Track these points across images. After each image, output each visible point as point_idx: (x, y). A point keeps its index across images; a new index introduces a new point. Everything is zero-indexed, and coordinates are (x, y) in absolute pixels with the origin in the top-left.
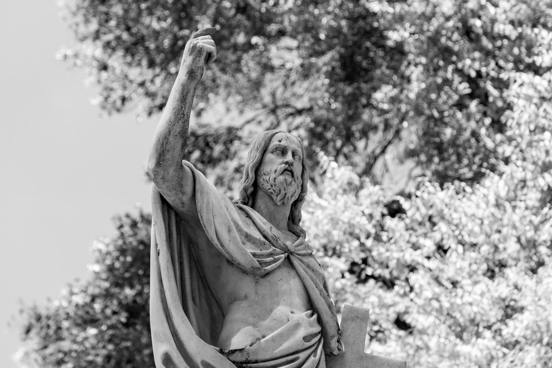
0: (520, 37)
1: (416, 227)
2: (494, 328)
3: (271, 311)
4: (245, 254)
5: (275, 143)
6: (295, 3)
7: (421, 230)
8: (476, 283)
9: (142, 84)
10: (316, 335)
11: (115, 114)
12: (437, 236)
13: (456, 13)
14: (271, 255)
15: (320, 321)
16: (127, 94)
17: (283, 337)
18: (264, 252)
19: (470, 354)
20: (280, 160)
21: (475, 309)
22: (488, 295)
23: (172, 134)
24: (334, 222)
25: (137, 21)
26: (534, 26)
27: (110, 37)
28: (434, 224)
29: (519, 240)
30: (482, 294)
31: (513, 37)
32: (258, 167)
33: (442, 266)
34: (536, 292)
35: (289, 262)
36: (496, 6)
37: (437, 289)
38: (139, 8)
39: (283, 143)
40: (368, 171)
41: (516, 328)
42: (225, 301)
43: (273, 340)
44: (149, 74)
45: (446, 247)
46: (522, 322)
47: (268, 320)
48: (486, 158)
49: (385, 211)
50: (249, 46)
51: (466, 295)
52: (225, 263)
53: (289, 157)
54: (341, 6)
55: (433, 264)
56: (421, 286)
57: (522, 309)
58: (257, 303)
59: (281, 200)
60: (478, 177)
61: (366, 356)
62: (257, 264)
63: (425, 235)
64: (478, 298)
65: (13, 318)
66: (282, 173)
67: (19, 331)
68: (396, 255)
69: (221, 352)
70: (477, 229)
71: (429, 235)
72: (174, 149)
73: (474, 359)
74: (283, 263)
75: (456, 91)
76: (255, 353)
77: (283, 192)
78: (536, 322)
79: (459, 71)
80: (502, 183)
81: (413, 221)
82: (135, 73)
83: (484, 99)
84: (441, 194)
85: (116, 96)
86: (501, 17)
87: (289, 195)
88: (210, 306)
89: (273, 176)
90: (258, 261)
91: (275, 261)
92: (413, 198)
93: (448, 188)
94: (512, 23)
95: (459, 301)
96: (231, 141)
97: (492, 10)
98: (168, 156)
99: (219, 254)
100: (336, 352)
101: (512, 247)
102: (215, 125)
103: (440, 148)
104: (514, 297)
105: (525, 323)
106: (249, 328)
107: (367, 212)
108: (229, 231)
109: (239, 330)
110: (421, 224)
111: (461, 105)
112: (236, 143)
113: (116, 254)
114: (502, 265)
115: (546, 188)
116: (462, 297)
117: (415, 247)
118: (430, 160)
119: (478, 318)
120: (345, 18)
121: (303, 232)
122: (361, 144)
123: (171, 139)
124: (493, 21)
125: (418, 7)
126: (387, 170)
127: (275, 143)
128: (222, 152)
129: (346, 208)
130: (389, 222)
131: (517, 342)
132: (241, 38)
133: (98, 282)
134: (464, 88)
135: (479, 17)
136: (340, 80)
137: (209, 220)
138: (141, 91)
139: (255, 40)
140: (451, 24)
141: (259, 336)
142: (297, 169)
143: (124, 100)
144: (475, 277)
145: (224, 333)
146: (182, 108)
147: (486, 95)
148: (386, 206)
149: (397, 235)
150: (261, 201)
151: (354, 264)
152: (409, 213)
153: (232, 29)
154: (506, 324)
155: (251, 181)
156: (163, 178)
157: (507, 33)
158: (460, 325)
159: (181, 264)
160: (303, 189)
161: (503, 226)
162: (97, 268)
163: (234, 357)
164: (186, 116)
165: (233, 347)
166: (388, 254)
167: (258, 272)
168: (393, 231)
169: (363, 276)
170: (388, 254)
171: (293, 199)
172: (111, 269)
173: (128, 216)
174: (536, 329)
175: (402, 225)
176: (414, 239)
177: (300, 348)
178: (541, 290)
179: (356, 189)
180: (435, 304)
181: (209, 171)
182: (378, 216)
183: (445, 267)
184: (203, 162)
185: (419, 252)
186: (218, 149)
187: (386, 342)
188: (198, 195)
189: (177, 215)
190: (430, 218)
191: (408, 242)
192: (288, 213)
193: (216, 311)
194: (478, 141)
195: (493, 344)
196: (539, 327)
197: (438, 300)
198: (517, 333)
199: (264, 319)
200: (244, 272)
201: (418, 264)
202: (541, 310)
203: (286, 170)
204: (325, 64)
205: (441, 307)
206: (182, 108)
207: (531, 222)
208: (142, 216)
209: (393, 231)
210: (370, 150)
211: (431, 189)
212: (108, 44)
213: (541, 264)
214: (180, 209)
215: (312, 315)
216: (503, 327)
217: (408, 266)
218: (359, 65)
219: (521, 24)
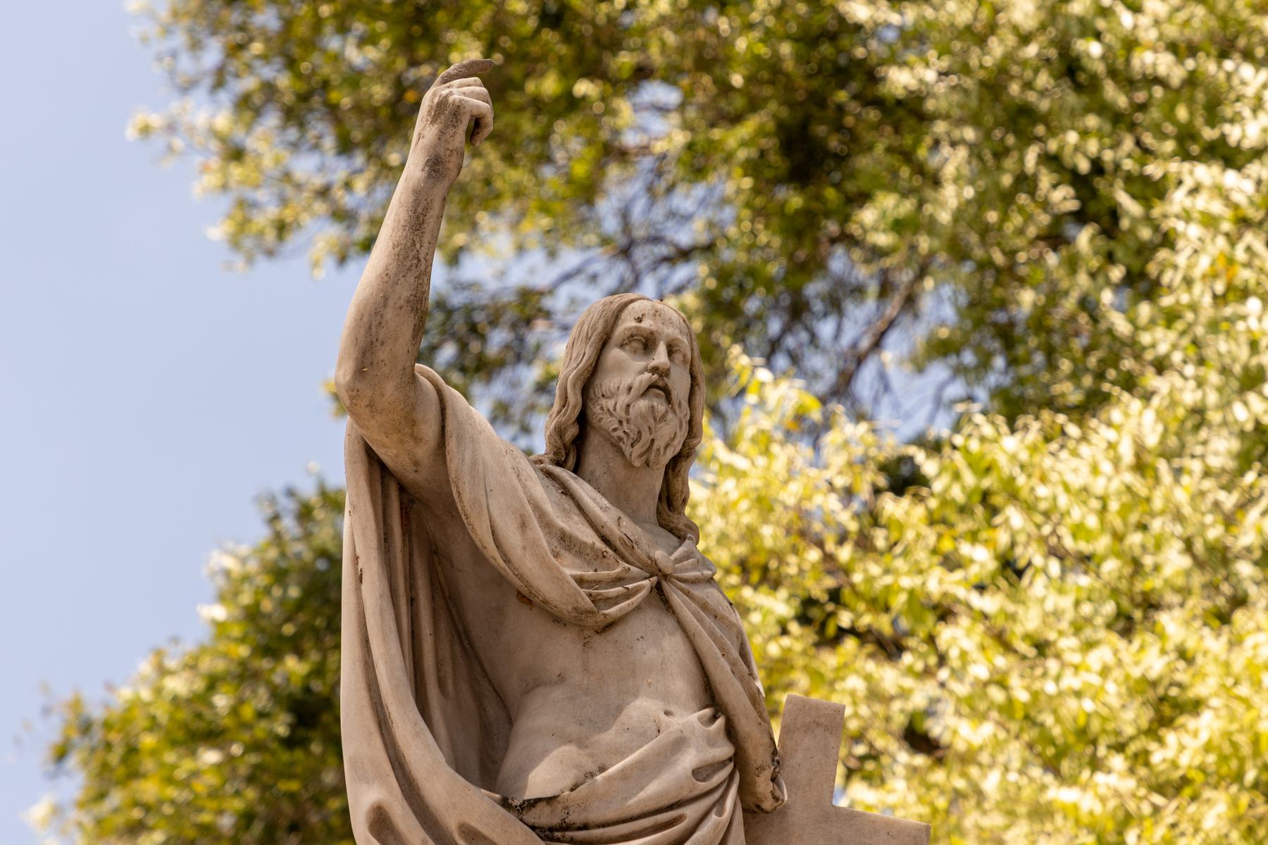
0: (1192, 80)
1: (953, 516)
2: (1133, 748)
3: (620, 709)
4: (559, 578)
5: (627, 323)
7: (963, 526)
8: (1090, 645)
9: (324, 193)
10: (723, 764)
11: (263, 264)
12: (1003, 538)
13: (1043, 27)
14: (618, 580)
15: (731, 732)
16: (288, 215)
17: (646, 770)
18: (603, 573)
19: (1076, 807)
20: (640, 364)
21: (1088, 705)
22: (1117, 674)
23: (391, 302)
25: (311, 44)
26: (1223, 55)
27: (249, 83)
28: (994, 511)
30: (1105, 672)
33: (1011, 608)
34: (1227, 665)
35: (659, 595)
36: (1136, 9)
37: (1001, 661)
39: (647, 324)
40: (842, 389)
41: (1182, 748)
43: (624, 775)
44: (339, 169)
46: (1195, 734)
47: (612, 731)
48: (1113, 360)
49: (882, 481)
50: (570, 104)
51: (1068, 673)
52: (514, 601)
53: (660, 357)
54: (778, 12)
55: (989, 603)
56: (964, 655)
57: (1196, 706)
59: (641, 455)
60: (1094, 403)
63: (974, 537)
64: (1095, 680)
66: (644, 394)
67: (40, 756)
68: (906, 582)
69: (505, 803)
70: (1092, 522)
71: (984, 535)
72: (397, 339)
73: (1085, 819)
74: (647, 601)
75: (1045, 205)
77: (646, 437)
78: (1227, 735)
79: (1052, 160)
80: (1149, 416)
81: (945, 502)
82: (305, 167)
84: (1011, 443)
86: (1151, 35)
87: (659, 444)
88: (478, 698)
89: (623, 399)
90: (590, 595)
91: (628, 595)
92: (947, 450)
93: (1026, 428)
94: (1173, 47)
95: (1050, 687)
96: (528, 322)
97: (1126, 18)
98: (383, 354)
99: (500, 580)
100: (768, 804)
101: (1175, 562)
102: (492, 285)
103: (1007, 336)
104: (1179, 677)
105: (1204, 737)
106: (569, 750)
107: (840, 482)
108: (523, 525)
110: (964, 510)
111: (1055, 238)
112: (540, 326)
114: (1151, 604)
115: (1249, 427)
116: (1057, 679)
117: (951, 563)
119: (1095, 726)
120: (788, 37)
122: (826, 329)
123: (389, 314)
124: (1131, 44)
126: (887, 387)
127: (627, 323)
128: (507, 347)
130: (892, 506)
131: (1185, 781)
132: (550, 85)
133: (222, 647)
135: (1098, 36)
136: (778, 181)
138: (320, 207)
139: (583, 88)
140: (1032, 50)
141: (591, 766)
142: (679, 383)
143: (282, 228)
144: (1088, 633)
146: (414, 244)
147: (1114, 213)
148: (883, 468)
149: (910, 535)
150: (596, 457)
152: (938, 486)
153: (533, 64)
155: (573, 412)
156: (371, 405)
157: (1162, 70)
158: (1052, 741)
159: (412, 601)
160: (693, 431)
162: (219, 612)
163: (535, 816)
164: (423, 261)
165: (530, 794)
166: (888, 580)
167: (590, 621)
168: (901, 527)
169: (831, 630)
170: (888, 580)
171: (670, 454)
172: (252, 615)
173: (291, 493)
174: (1227, 749)
175: (919, 512)
176: (947, 545)
177: (686, 794)
178: (1239, 662)
180: (997, 694)
181: (477, 389)
182: (864, 492)
183: (1020, 610)
184: (463, 369)
185: (958, 575)
188: (452, 444)
189: (402, 489)
191: (934, 551)
193: (492, 710)
195: (1129, 784)
196: (1235, 745)
198: (1184, 760)
199: (604, 728)
200: (557, 620)
201: (957, 601)
202: (1239, 708)
203: (652, 386)
204: (743, 144)
205: (1010, 701)
206: (414, 244)
207: (1217, 505)
209: (901, 527)
210: (846, 340)
211: (988, 430)
213: (1239, 601)
214: (409, 474)
215: (714, 718)
216: (1153, 746)
219: (1192, 50)
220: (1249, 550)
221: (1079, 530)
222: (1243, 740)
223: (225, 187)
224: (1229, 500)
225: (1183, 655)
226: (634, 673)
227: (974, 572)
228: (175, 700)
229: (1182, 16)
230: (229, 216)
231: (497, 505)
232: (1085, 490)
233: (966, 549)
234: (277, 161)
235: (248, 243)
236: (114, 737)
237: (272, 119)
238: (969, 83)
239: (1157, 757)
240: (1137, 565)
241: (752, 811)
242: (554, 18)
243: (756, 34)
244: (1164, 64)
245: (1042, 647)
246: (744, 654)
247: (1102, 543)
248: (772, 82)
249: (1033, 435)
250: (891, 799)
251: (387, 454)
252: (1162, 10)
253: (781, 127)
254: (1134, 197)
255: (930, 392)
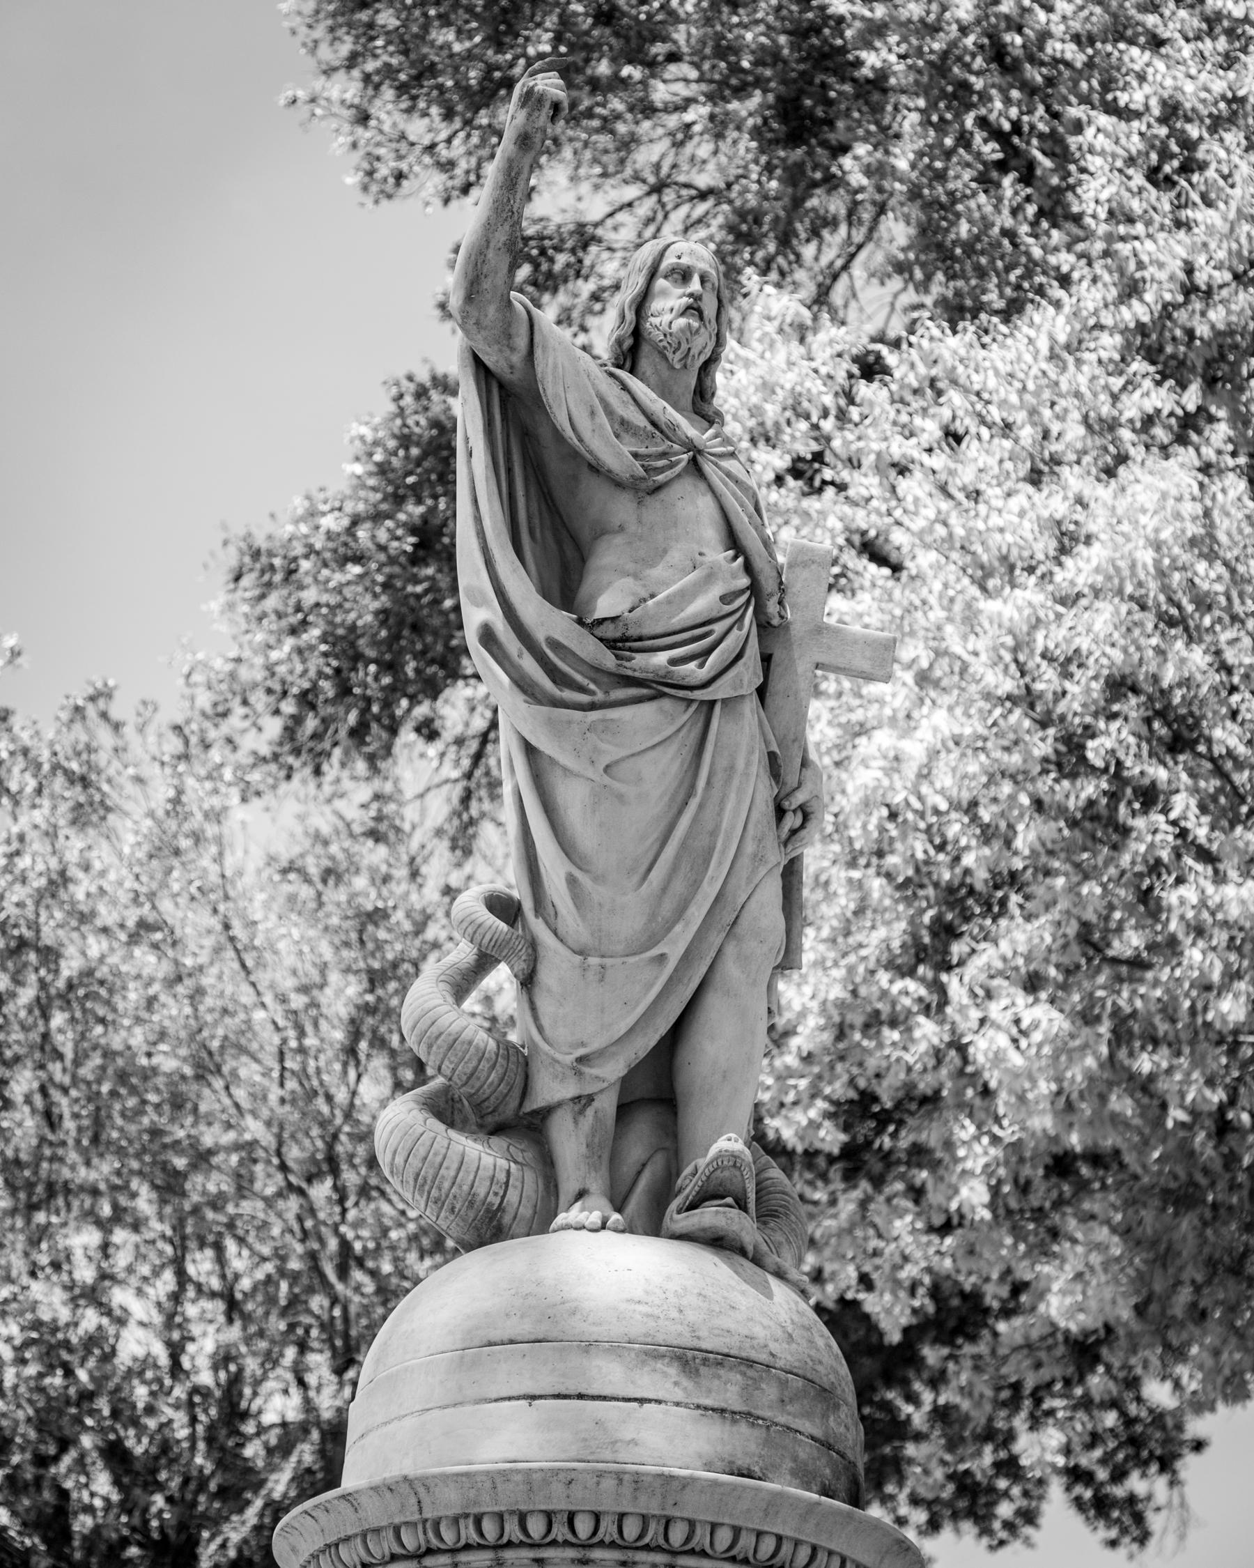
0: (1090, 64)
1: (909, 397)
3: (665, 551)
4: (619, 454)
5: (669, 261)
6: (697, 5)
7: (917, 404)
9: (431, 148)
11: (385, 203)
12: (946, 413)
13: (978, 22)
14: (664, 455)
15: (748, 568)
16: (404, 166)
17: (685, 596)
18: (652, 450)
19: (1000, 614)
20: (680, 291)
21: (1009, 538)
22: (1031, 515)
24: (768, 388)
25: (422, 37)
27: (371, 66)
28: (939, 393)
29: (1086, 420)
30: (1022, 514)
31: (1079, 65)
32: (641, 304)
33: (952, 465)
35: (695, 467)
36: (1049, 9)
37: (945, 505)
38: (425, 15)
39: (685, 261)
40: (821, 298)
42: (585, 534)
43: (669, 601)
45: (961, 431)
46: (1088, 560)
48: (1028, 275)
49: (855, 370)
50: (618, 83)
51: (994, 516)
52: (585, 469)
53: (695, 285)
54: (778, 9)
55: (938, 461)
56: (916, 500)
57: (1088, 540)
58: (641, 538)
60: (1012, 310)
61: (828, 628)
62: (641, 472)
64: (1016, 520)
65: (212, 554)
66: (683, 314)
67: (224, 576)
68: (875, 446)
69: (580, 622)
70: (1014, 399)
71: (932, 411)
73: (1007, 623)
74: (685, 469)
75: (978, 155)
76: (638, 623)
77: (684, 346)
78: (1112, 562)
79: (982, 122)
80: (1061, 320)
82: (417, 129)
83: (1028, 175)
84: (953, 341)
85: (383, 171)
86: (1059, 29)
87: (695, 351)
88: (559, 543)
89: (667, 318)
91: (672, 465)
92: (904, 346)
94: (1076, 38)
95: (981, 525)
96: (585, 247)
97: (1042, 16)
98: (486, 285)
99: (575, 455)
101: (1075, 432)
102: (557, 219)
104: (1076, 517)
105: (1094, 563)
106: (629, 582)
107: (823, 370)
109: (610, 584)
110: (915, 392)
111: (986, 182)
112: (593, 249)
113: (392, 444)
114: (1055, 461)
115: (1132, 325)
117: (909, 433)
118: (928, 277)
119: (1015, 553)
120: (785, 32)
121: (719, 414)
122: (808, 251)
123: (491, 254)
124: (1044, 35)
125: (914, 10)
126: (854, 295)
127: (669, 261)
128: (568, 265)
129: (791, 364)
130: (864, 390)
131: (1079, 595)
132: (603, 68)
133: (362, 493)
134: (991, 150)
135: (1020, 30)
136: (777, 142)
137: (556, 395)
138: (427, 159)
139: (626, 71)
140: (970, 41)
141: (644, 594)
142: (709, 307)
143: (400, 176)
144: (1009, 484)
145: (585, 590)
147: (1031, 165)
148: (856, 360)
149: (877, 411)
150: (647, 362)
151: (799, 459)
152: (897, 374)
153: (589, 50)
154: (1060, 564)
155: (628, 328)
156: (477, 323)
157: (1068, 56)
158: (982, 567)
159: (509, 471)
160: (719, 342)
161: (1060, 395)
162: (359, 469)
163: (600, 631)
165: (598, 615)
167: (643, 486)
168: (872, 404)
169: (817, 483)
171: (703, 359)
172: (383, 470)
173: (410, 378)
174: (1111, 571)
176: (904, 418)
177: (715, 614)
178: (1122, 505)
179: (801, 333)
180: (941, 531)
181: (546, 298)
182: (841, 376)
184: (535, 283)
185: (914, 441)
186: (561, 259)
187: (853, 594)
188: (538, 353)
189: (501, 386)
190: (933, 382)
192: (693, 382)
193: (570, 552)
194: (1015, 245)
195: (1038, 598)
196: (1117, 569)
197: (945, 524)
198: (1080, 581)
200: (618, 484)
202: (1120, 540)
203: (689, 307)
205: (951, 535)
207: (1106, 387)
208: (434, 379)
210: (824, 261)
211: (936, 332)
212: (367, 78)
213: (1122, 459)
214: (507, 375)
215: (735, 558)
216: (1056, 569)
217: (894, 465)
218: (811, 116)
219: (1091, 41)
220: (1131, 421)
221: (1003, 404)
222: (1122, 564)
223: (354, 145)
224: (1117, 383)
225: (1080, 501)
226: (675, 524)
227: (925, 439)
228: (329, 535)
229: (1086, 12)
230: (357, 169)
231: (572, 398)
232: (1011, 375)
233: (918, 421)
234: (394, 125)
235: (374, 188)
236: (277, 562)
237: (388, 93)
238: (921, 63)
239: (1059, 576)
240: (1046, 435)
241: (764, 626)
242: (606, 16)
243: (762, 28)
244: (1070, 51)
245: (975, 495)
246: (757, 509)
247: (1020, 417)
248: (774, 65)
249: (970, 336)
250: (860, 608)
251: (490, 360)
252: (1069, 9)
253: (779, 98)
254: (1044, 153)
255: (889, 299)
